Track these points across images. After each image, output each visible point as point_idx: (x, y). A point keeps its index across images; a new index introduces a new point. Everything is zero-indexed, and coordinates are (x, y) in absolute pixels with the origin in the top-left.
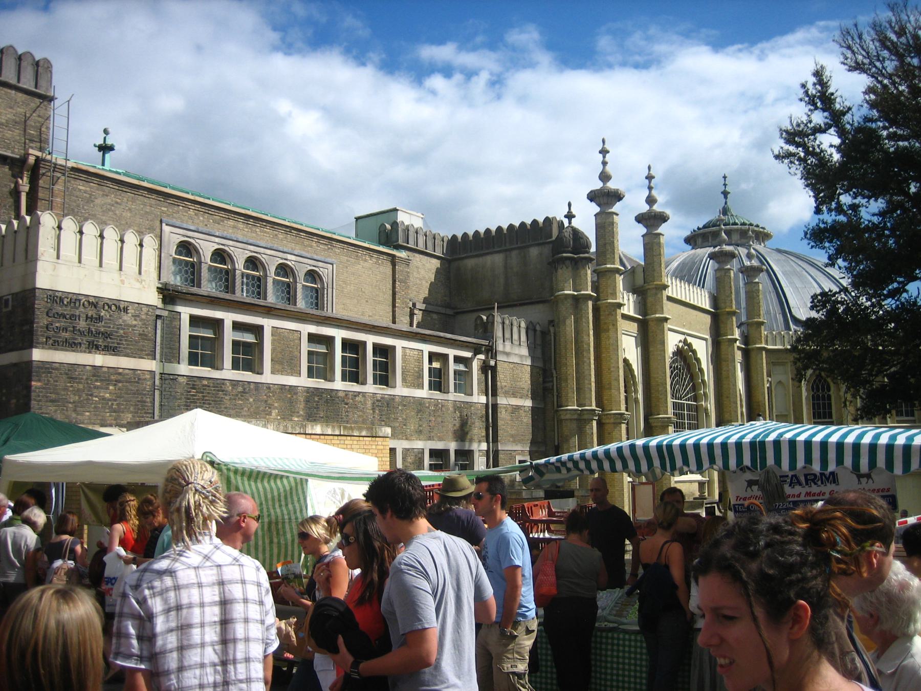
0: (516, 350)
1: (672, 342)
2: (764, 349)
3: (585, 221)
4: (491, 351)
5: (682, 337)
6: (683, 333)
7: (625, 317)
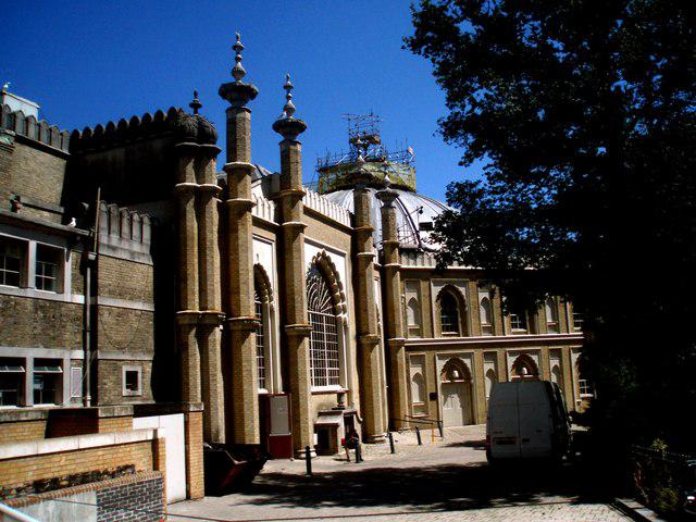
0: (125, 245)
1: (309, 254)
2: (398, 268)
3: (215, 114)
4: (89, 244)
5: (321, 251)
6: (321, 246)
7: (258, 223)
